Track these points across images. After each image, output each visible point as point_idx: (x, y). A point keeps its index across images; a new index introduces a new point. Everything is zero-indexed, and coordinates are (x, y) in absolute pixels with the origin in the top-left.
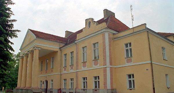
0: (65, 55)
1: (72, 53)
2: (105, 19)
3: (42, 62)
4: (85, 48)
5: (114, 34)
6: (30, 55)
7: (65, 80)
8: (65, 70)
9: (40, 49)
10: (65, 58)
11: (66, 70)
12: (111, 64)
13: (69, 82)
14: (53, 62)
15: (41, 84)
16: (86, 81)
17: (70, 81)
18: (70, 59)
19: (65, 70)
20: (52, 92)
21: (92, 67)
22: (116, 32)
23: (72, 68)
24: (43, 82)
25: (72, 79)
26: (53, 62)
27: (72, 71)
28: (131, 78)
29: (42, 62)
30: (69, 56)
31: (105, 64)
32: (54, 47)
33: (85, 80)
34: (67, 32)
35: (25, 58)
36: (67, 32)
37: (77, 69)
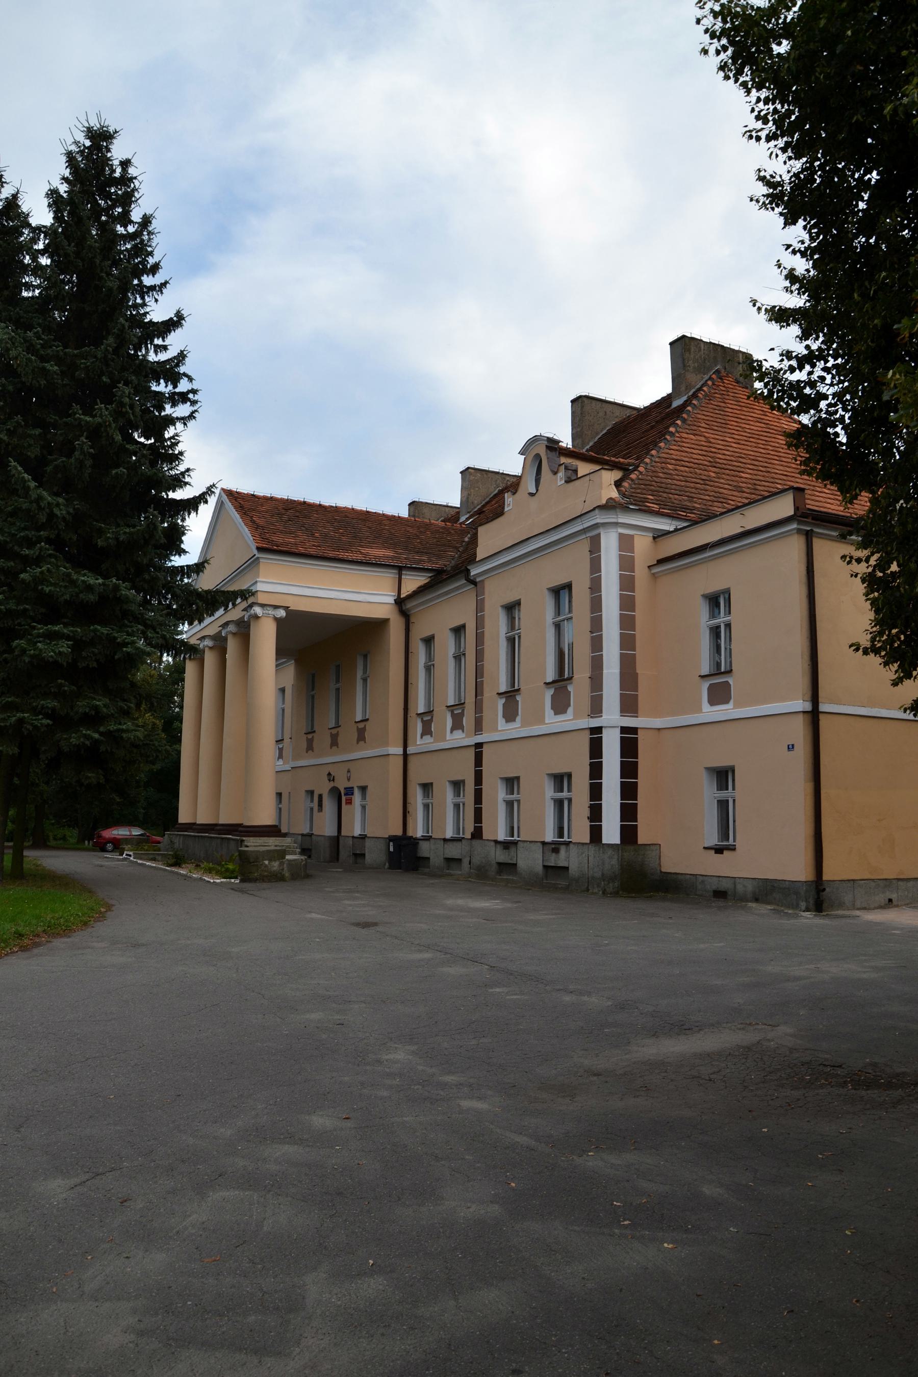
0: (512, 608)
1: (459, 631)
2: (676, 403)
3: (313, 676)
4: (565, 595)
5: (658, 536)
6: (232, 646)
7: (512, 783)
8: (510, 715)
9: (282, 613)
10: (558, 612)
11: (462, 729)
12: (629, 705)
13: (540, 799)
14: (365, 680)
15: (312, 809)
16: (565, 794)
17: (549, 792)
18: (451, 663)
19: (427, 731)
20: (364, 855)
21: (444, 740)
22: (668, 521)
23: (457, 725)
24: (320, 797)
25: (561, 780)
26: (365, 680)
27: (553, 722)
28: (727, 789)
29: (313, 676)
30: (446, 646)
31: (596, 708)
32: (363, 594)
33: (562, 791)
34: (468, 474)
35: (210, 659)
36: (468, 474)
37: (478, 727)
